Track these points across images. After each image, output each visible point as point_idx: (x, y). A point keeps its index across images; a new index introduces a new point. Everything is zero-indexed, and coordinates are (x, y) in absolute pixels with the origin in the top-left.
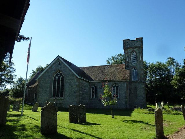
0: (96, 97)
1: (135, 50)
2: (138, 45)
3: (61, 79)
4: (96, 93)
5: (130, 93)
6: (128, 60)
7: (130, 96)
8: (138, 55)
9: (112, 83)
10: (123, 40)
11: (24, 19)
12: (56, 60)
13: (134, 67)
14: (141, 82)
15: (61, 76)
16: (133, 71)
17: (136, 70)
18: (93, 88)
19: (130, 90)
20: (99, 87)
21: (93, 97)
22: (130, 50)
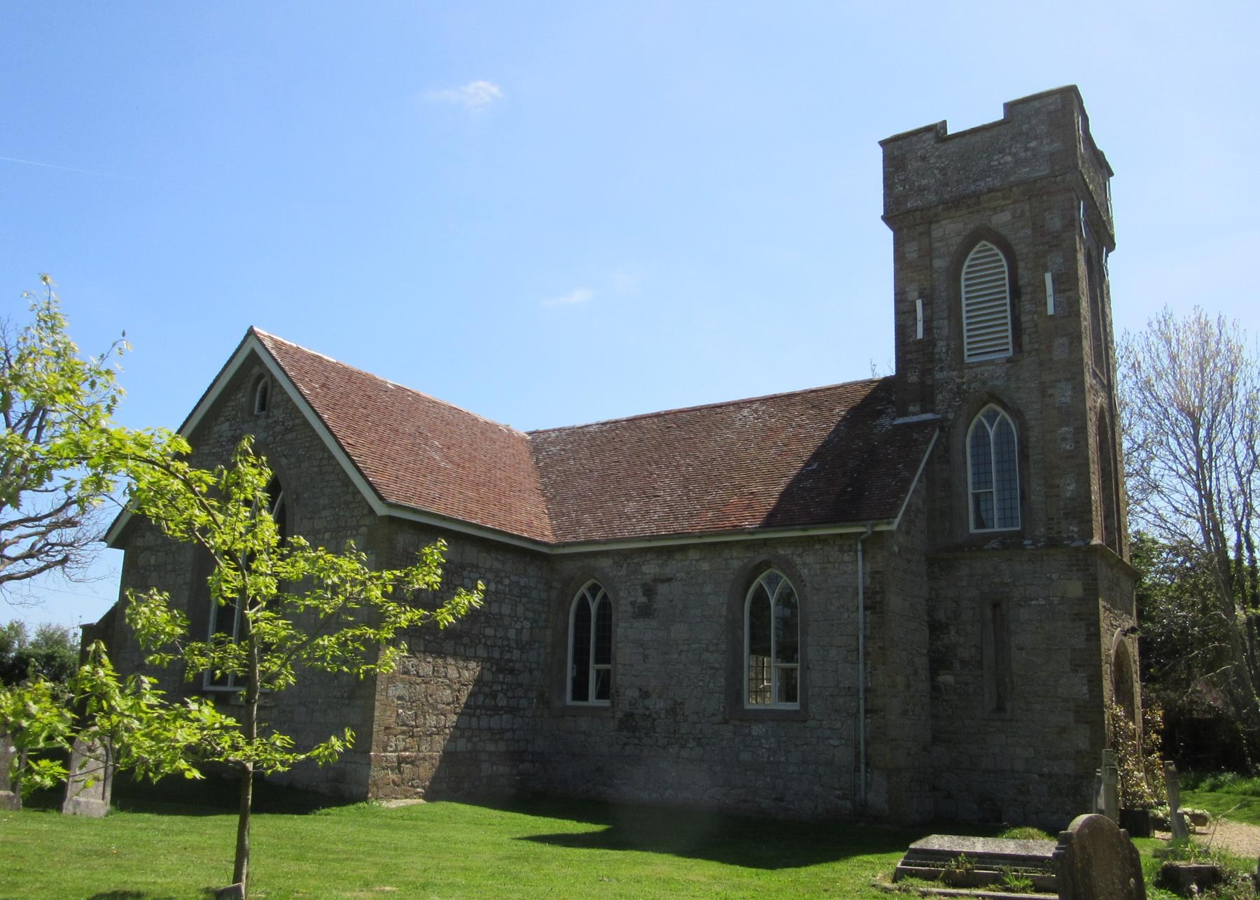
0: (601, 694)
1: (1001, 219)
3: (593, 608)
4: (604, 654)
5: (938, 662)
6: (927, 330)
7: (935, 688)
8: (1025, 276)
9: (737, 561)
10: (883, 144)
11: (1010, 107)
12: (824, 525)
13: (993, 397)
14: (1054, 543)
15: (594, 597)
16: (981, 435)
17: (1003, 431)
18: (583, 604)
19: (936, 628)
20: (626, 599)
21: (580, 692)
22: (950, 229)
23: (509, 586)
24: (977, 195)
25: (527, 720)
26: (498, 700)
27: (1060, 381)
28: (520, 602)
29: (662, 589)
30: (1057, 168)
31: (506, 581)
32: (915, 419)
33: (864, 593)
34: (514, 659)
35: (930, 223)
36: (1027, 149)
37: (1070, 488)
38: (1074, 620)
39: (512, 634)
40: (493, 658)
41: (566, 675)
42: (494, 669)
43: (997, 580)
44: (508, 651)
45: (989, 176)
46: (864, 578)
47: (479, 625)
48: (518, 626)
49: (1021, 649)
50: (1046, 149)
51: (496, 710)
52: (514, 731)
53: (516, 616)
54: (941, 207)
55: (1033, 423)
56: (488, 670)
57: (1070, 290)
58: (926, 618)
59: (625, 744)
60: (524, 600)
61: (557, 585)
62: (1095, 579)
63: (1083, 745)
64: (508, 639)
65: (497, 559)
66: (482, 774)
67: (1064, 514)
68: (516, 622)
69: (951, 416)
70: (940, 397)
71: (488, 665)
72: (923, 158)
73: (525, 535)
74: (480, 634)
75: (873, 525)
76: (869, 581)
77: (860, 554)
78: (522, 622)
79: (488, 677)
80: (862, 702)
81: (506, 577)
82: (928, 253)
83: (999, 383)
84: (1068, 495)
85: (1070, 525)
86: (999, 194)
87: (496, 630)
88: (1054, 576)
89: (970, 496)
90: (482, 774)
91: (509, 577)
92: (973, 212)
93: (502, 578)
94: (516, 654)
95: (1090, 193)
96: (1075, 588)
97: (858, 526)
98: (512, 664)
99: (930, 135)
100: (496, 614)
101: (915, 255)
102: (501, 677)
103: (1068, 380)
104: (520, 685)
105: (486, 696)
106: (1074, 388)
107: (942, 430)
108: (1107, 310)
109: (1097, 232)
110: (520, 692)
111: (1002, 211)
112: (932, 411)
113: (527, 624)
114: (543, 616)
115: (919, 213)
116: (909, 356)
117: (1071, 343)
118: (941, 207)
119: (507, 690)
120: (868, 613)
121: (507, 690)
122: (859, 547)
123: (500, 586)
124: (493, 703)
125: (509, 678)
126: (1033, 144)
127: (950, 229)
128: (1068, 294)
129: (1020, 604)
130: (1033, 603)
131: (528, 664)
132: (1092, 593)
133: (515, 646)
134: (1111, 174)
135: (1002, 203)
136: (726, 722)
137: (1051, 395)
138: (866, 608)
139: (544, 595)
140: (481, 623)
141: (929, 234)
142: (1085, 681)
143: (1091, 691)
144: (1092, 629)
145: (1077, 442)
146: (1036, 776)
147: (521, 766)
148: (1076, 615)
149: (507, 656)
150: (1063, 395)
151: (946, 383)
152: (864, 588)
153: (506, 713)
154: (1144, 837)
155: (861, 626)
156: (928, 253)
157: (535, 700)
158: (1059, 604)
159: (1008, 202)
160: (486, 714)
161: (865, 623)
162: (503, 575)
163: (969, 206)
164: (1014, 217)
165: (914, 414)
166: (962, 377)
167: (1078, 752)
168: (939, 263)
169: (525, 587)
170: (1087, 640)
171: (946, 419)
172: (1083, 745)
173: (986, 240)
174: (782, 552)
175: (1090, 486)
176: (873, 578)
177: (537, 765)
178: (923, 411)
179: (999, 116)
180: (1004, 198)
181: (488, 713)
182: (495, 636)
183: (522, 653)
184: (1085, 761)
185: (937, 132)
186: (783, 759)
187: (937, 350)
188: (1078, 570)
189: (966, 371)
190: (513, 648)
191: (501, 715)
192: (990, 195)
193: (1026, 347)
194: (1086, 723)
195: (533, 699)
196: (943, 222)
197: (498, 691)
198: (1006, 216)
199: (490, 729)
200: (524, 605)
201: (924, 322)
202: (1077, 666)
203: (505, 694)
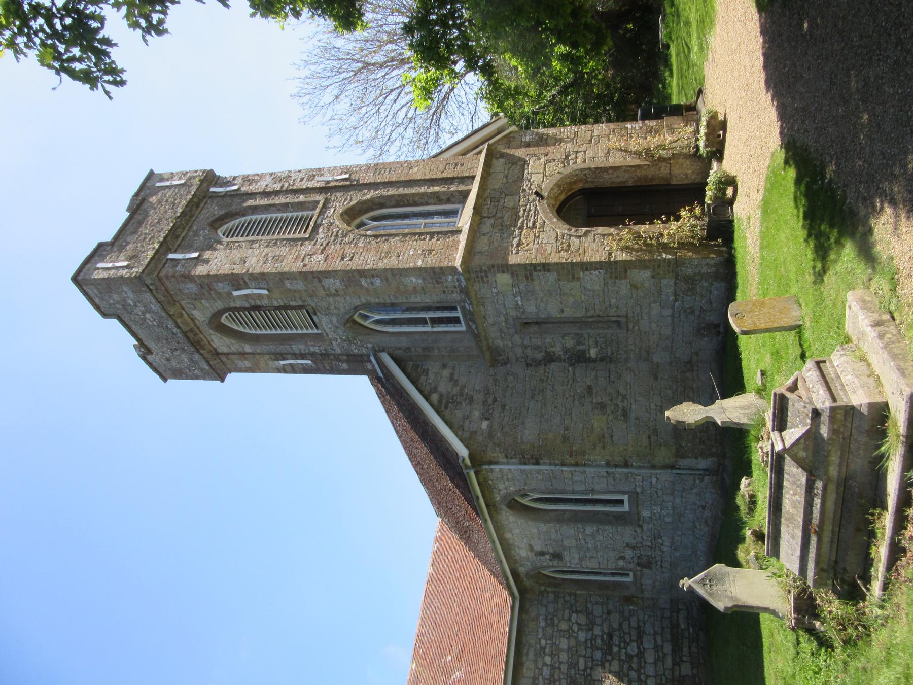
2: (155, 307)
6: (303, 356)
7: (602, 360)
11: (105, 315)
23: (546, 639)
24: (185, 334)
25: (646, 617)
26: (632, 653)
27: (323, 287)
28: (557, 626)
29: (538, 548)
30: (144, 289)
31: (543, 642)
32: (377, 366)
33: (525, 464)
34: (600, 634)
35: (218, 354)
36: (135, 306)
37: (414, 280)
38: (532, 279)
39: (582, 636)
40: (601, 658)
41: (609, 581)
42: (609, 657)
43: (503, 324)
44: (595, 640)
45: (167, 327)
46: (513, 464)
47: (577, 676)
48: (575, 628)
49: (562, 311)
50: (131, 295)
51: (641, 654)
52: (655, 634)
53: (568, 631)
54: (202, 352)
55: (363, 301)
56: (610, 665)
57: (243, 278)
58: (541, 370)
59: (662, 566)
60: (556, 621)
61: (543, 588)
62: (493, 266)
63: (647, 274)
64: (586, 641)
65: (527, 654)
66: (690, 674)
67: (438, 284)
68: (573, 631)
69: (370, 345)
70: (356, 351)
71: (607, 664)
72: (168, 360)
73: (507, 629)
74: (584, 675)
75: (467, 467)
76: (513, 460)
77: (492, 467)
78: (573, 623)
79: (615, 666)
80: (619, 470)
81: (540, 644)
82: (243, 355)
83: (334, 319)
84: (420, 281)
85: (447, 280)
86: (179, 321)
87: (580, 656)
88: (495, 291)
89: (435, 329)
90: (690, 674)
91: (540, 640)
92: (201, 332)
93: (541, 648)
94: (597, 631)
95: (162, 244)
96: (504, 279)
97: (470, 478)
98: (605, 636)
99: (149, 357)
100: (568, 656)
101: (246, 362)
102: (615, 649)
103: (320, 281)
104: (621, 625)
105: (630, 668)
106: (326, 278)
107: (383, 350)
108: (260, 186)
109: (198, 205)
110: (625, 626)
111: (192, 315)
112: (368, 356)
113: (574, 615)
114: (567, 598)
115: (211, 363)
116: (328, 367)
117: (288, 279)
118: (202, 352)
119: (625, 642)
120: (542, 462)
121: (625, 642)
122: (485, 467)
123: (547, 651)
124: (635, 658)
125: (616, 640)
126: (131, 303)
127: (220, 343)
128: (247, 281)
129: (523, 312)
130: (520, 303)
131: (604, 616)
132: (506, 268)
133: (591, 633)
134: (151, 174)
135: (186, 316)
136: (641, 526)
137: (337, 291)
138: (537, 463)
139: (551, 596)
140: (576, 674)
141: (227, 354)
142: (588, 273)
143: (596, 269)
144: (538, 268)
145: (373, 276)
146: (677, 304)
147: (682, 627)
148: (527, 278)
149: (599, 641)
150: (334, 284)
151: (343, 347)
152: (521, 464)
153: (642, 643)
154: (733, 226)
155: (553, 468)
156: (243, 355)
157: (631, 607)
158: (519, 288)
159: (184, 312)
160: (644, 668)
161: (550, 464)
162: (538, 646)
163: (196, 334)
164: (195, 308)
165: (374, 366)
166: (337, 339)
167: (653, 277)
168: (248, 348)
169: (546, 619)
170: (549, 271)
171: (373, 347)
172: (647, 274)
173: (221, 318)
174: (498, 499)
175: (409, 269)
176: (511, 458)
177: (680, 607)
178: (370, 361)
179: (115, 322)
180: (182, 315)
181: (643, 665)
182: (585, 656)
183: (595, 623)
184: (662, 273)
185: (145, 351)
186: (670, 504)
187: (318, 351)
188: (487, 277)
189: (330, 336)
190: (593, 635)
191: (644, 649)
192: (181, 325)
193: (300, 303)
194: (626, 271)
195: (630, 610)
196: (215, 346)
197: (626, 653)
198: (196, 313)
199: (655, 663)
200: (560, 621)
201: (297, 359)
202: (573, 277)
203: (628, 644)
